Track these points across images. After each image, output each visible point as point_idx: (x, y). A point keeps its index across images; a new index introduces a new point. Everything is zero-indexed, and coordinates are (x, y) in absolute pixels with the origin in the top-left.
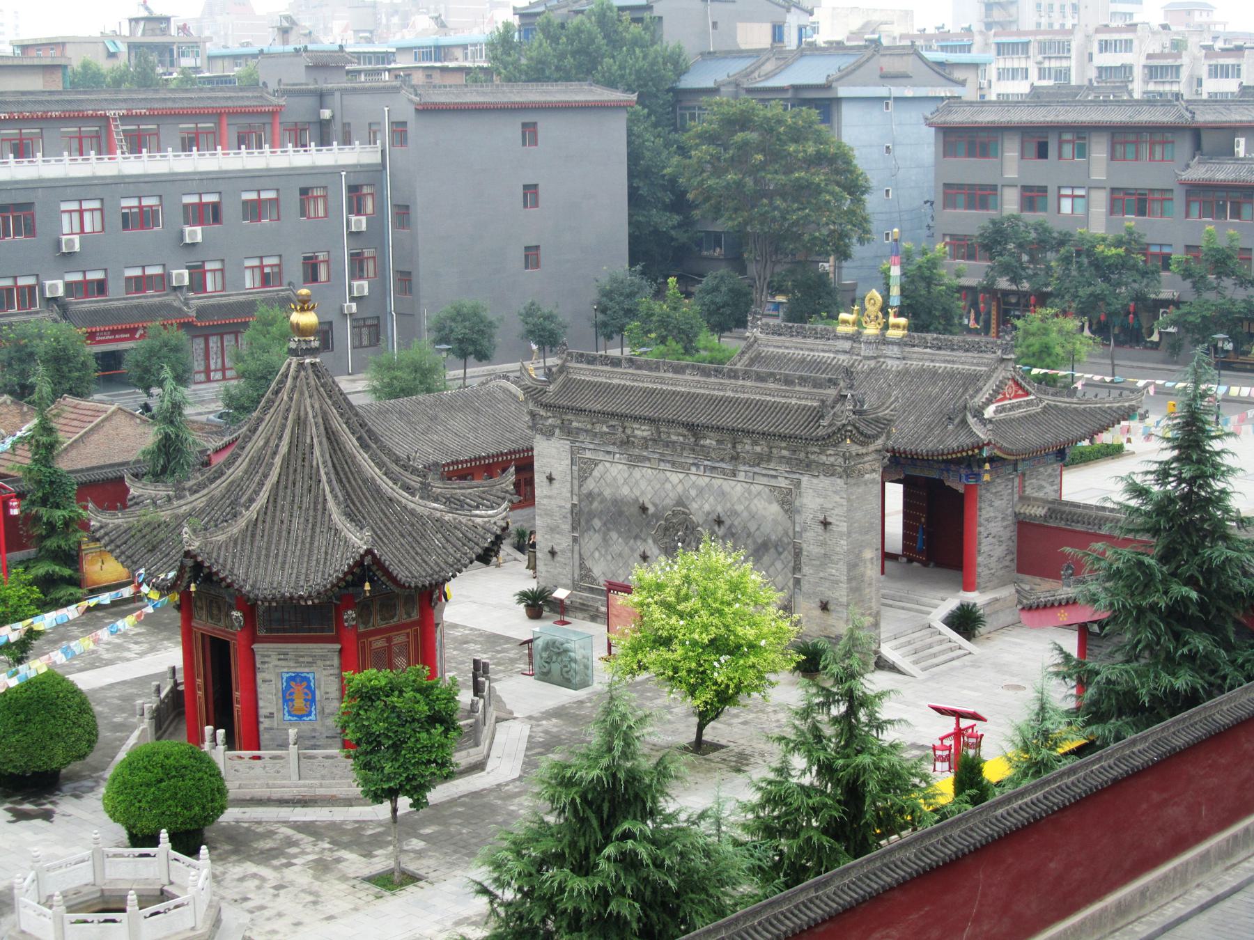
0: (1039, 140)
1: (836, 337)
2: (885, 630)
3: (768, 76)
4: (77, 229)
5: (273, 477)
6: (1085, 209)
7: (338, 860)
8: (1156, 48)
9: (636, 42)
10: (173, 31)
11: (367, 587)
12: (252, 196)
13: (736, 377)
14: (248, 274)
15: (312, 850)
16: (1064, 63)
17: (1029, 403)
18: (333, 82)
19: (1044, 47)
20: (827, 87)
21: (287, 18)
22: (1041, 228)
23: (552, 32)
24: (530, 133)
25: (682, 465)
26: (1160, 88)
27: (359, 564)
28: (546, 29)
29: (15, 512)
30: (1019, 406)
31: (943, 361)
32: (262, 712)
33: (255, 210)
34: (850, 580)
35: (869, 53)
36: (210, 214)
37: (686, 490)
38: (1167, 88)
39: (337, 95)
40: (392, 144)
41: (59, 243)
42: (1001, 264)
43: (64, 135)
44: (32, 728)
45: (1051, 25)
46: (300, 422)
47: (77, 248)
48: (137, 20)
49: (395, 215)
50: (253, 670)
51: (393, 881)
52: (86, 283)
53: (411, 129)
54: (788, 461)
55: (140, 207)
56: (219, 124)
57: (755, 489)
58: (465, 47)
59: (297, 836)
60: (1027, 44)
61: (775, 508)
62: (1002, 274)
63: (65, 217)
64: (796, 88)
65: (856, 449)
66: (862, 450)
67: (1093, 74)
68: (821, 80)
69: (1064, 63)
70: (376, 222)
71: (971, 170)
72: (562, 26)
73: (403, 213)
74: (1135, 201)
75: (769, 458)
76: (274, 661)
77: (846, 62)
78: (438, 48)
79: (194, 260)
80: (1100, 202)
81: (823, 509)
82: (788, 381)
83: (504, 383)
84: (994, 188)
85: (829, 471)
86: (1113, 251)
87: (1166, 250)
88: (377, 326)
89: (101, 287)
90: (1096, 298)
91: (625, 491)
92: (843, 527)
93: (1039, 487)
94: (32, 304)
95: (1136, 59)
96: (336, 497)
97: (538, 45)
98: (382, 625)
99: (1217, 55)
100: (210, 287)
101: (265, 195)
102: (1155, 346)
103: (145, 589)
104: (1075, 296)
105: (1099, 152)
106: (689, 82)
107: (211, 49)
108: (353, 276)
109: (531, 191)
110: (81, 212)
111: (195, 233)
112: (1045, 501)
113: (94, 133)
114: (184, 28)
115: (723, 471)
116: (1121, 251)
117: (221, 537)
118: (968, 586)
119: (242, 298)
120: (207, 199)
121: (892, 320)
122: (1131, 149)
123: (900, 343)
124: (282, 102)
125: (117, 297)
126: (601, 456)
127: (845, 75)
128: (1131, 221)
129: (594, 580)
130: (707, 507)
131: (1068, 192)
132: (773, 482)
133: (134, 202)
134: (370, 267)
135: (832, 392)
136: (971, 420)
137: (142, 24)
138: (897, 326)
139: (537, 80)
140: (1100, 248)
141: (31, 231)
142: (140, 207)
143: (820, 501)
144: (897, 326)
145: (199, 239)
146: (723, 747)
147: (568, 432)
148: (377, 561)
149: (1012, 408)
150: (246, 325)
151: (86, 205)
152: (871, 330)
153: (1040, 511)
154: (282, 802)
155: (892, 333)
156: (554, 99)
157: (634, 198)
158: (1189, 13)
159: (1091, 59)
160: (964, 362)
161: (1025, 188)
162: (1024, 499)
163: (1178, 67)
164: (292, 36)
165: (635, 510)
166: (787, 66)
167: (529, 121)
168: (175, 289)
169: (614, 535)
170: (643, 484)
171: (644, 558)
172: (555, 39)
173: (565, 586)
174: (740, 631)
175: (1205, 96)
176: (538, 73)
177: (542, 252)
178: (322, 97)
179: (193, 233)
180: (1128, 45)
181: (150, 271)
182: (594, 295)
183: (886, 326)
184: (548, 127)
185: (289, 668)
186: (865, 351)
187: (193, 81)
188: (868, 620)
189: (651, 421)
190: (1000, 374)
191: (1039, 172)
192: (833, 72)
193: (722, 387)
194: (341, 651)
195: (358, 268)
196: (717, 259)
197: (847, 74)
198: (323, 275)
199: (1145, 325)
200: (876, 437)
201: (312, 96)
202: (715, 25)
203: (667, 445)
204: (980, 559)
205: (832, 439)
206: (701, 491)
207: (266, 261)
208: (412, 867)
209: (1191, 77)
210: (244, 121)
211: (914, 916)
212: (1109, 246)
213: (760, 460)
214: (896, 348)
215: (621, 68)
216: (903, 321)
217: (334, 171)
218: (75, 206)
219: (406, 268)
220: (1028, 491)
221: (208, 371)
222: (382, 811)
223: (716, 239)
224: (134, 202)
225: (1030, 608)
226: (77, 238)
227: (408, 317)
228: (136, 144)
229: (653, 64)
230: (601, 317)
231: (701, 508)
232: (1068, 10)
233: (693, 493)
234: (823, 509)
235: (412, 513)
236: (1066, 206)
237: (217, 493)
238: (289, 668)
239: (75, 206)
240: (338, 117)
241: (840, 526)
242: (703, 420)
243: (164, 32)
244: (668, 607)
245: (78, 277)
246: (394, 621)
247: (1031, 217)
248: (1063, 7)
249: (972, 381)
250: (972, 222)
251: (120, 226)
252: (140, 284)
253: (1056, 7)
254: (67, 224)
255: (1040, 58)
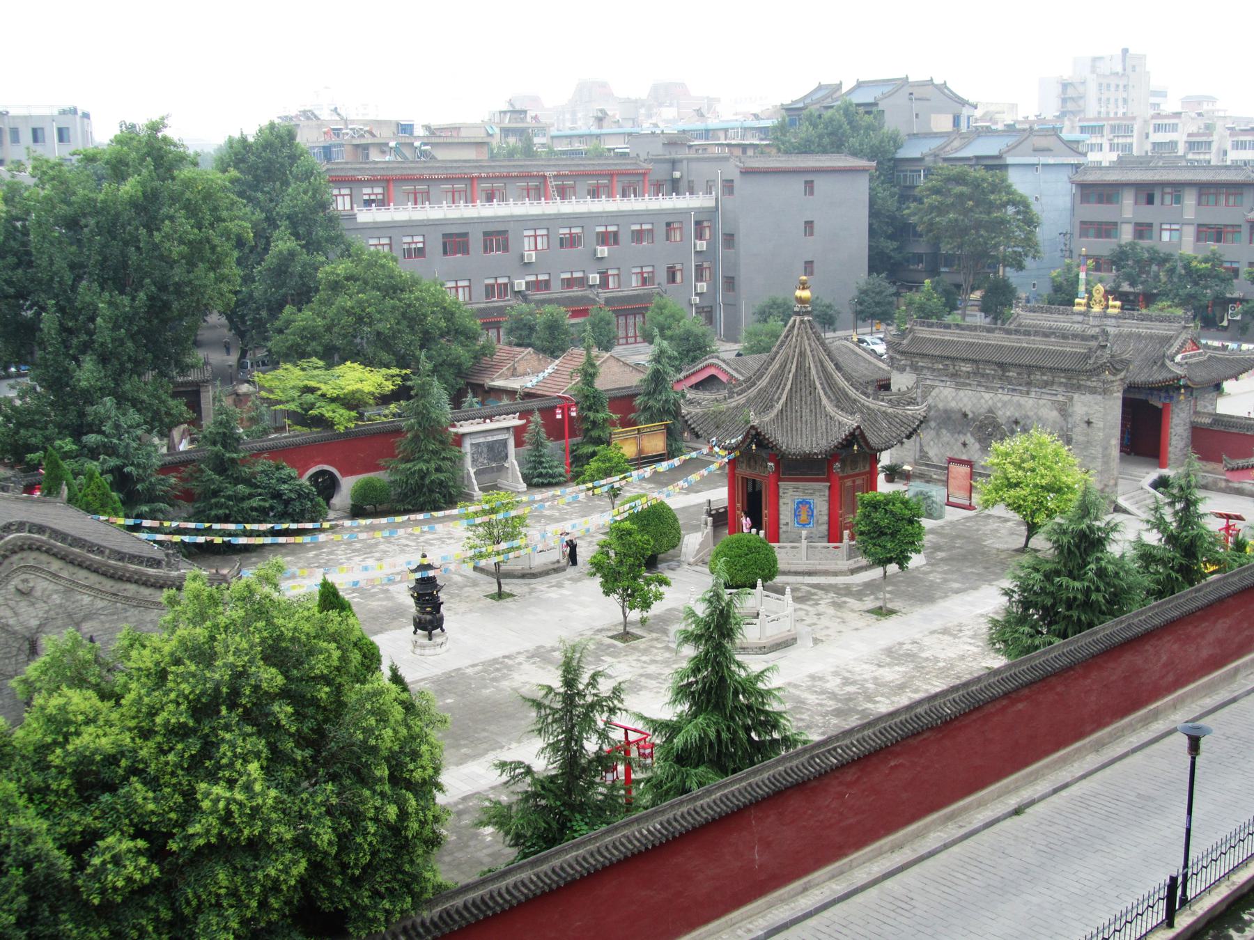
0: (1147, 193)
1: (1073, 313)
2: (1120, 489)
3: (957, 150)
4: (533, 247)
5: (788, 387)
6: (1179, 237)
7: (845, 602)
8: (1193, 129)
9: (869, 127)
10: (529, 119)
11: (856, 447)
12: (637, 227)
13: (1029, 335)
14: (634, 277)
15: (826, 600)
16: (1129, 140)
17: (1200, 354)
18: (682, 154)
19: (1114, 129)
20: (999, 157)
21: (601, 111)
22: (1151, 250)
23: (814, 120)
24: (809, 185)
25: (992, 388)
26: (1197, 157)
27: (852, 434)
28: (810, 118)
29: (574, 414)
30: (1194, 356)
31: (1143, 329)
32: (782, 522)
33: (639, 236)
34: (1104, 457)
35: (1026, 134)
36: (604, 239)
37: (995, 403)
38: (1202, 157)
39: (685, 162)
40: (723, 194)
41: (522, 256)
42: (1125, 273)
43: (404, 191)
44: (650, 528)
45: (1108, 113)
46: (802, 354)
47: (534, 259)
48: (505, 112)
49: (724, 240)
50: (777, 497)
51: (882, 612)
52: (538, 282)
53: (737, 184)
54: (1065, 385)
55: (571, 234)
56: (611, 181)
57: (1042, 402)
58: (726, 130)
59: (813, 591)
60: (1102, 127)
61: (1055, 414)
62: (1126, 280)
63: (526, 240)
64: (978, 158)
65: (1111, 378)
66: (1113, 378)
67: (1149, 147)
68: (996, 153)
69: (1129, 140)
70: (712, 244)
71: (1098, 212)
72: (820, 116)
73: (730, 239)
74: (1218, 233)
75: (1053, 383)
76: (790, 492)
77: (1011, 141)
78: (707, 131)
79: (602, 267)
80: (1189, 234)
81: (1087, 414)
82: (1064, 337)
83: (848, 344)
84: (1115, 224)
85: (1093, 391)
86: (1204, 265)
87: (1235, 265)
88: (711, 312)
89: (547, 284)
90: (1192, 297)
91: (953, 404)
92: (1101, 425)
93: (1203, 406)
94: (506, 295)
95: (1180, 137)
96: (829, 397)
97: (804, 131)
98: (851, 472)
99: (1237, 135)
100: (611, 286)
101: (645, 227)
102: (1225, 328)
103: (716, 449)
104: (1177, 295)
105: (1190, 200)
106: (902, 154)
107: (554, 132)
108: (697, 280)
109: (809, 225)
110: (536, 237)
111: (603, 251)
112: (1211, 414)
113: (537, 187)
114: (535, 118)
115: (1021, 392)
116: (1209, 265)
117: (767, 419)
118: (1162, 466)
119: (630, 293)
120: (610, 229)
121: (1111, 303)
122: (1212, 198)
123: (1115, 317)
124: (650, 166)
125: (556, 290)
126: (937, 383)
127: (1011, 149)
128: (1213, 246)
129: (929, 459)
130: (1008, 414)
131: (1167, 227)
132: (1054, 398)
133: (567, 231)
134: (707, 274)
135: (1094, 344)
136: (1168, 363)
137: (508, 115)
138: (1114, 307)
139: (805, 152)
140: (1194, 263)
141: (506, 249)
142: (571, 234)
143: (1085, 409)
144: (1114, 307)
145: (606, 255)
146: (868, 611)
147: (915, 368)
148: (862, 432)
149: (1191, 357)
150: (646, 309)
151: (538, 232)
152: (1097, 309)
153: (1207, 421)
154: (796, 573)
155: (1110, 311)
156: (822, 165)
157: (872, 232)
158: (1200, 103)
159: (1147, 137)
160: (1160, 329)
161: (1137, 224)
162: (1196, 413)
163: (1210, 143)
164: (605, 124)
165: (959, 416)
166: (969, 143)
167: (809, 178)
168: (591, 286)
169: (944, 431)
170: (965, 400)
171: (965, 445)
172: (815, 126)
173: (909, 464)
174: (1064, 479)
175: (1229, 163)
176: (805, 148)
177: (815, 265)
178: (674, 163)
179: (603, 251)
180: (1174, 128)
181: (576, 275)
182: (856, 293)
183: (1107, 307)
184: (820, 183)
185: (799, 496)
186: (1092, 321)
187: (556, 153)
188: (1112, 482)
189: (974, 361)
190: (1183, 336)
191: (1147, 214)
192: (1003, 147)
193: (1019, 341)
194: (830, 487)
195: (699, 277)
196: (920, 271)
197: (1014, 148)
198: (678, 278)
199: (1218, 315)
200: (1120, 371)
201: (668, 165)
202: (917, 115)
203: (983, 376)
204: (1170, 449)
205: (1096, 371)
206: (1004, 404)
207: (645, 270)
208: (889, 606)
209: (1219, 149)
210: (626, 179)
211: (1237, 614)
212: (1200, 262)
213: (1046, 384)
214: (1113, 320)
215: (861, 144)
216: (1118, 303)
217: (686, 212)
218: (532, 233)
219: (731, 275)
220: (1199, 409)
221: (627, 337)
222: (877, 572)
223: (919, 258)
224: (567, 231)
225: (1233, 470)
226: (533, 253)
227: (732, 307)
228: (563, 193)
229: (882, 142)
230: (859, 308)
231: (1004, 415)
232: (1120, 103)
233: (999, 405)
234: (1087, 414)
235: (868, 408)
236: (1166, 236)
237: (752, 395)
238: (799, 496)
239: (532, 233)
240: (685, 178)
241: (1098, 424)
242: (1009, 360)
243: (523, 120)
244: (1019, 467)
245: (533, 278)
246: (857, 471)
247: (1145, 243)
248: (1116, 100)
249: (1167, 340)
250: (1104, 247)
251: (482, 250)
252: (569, 283)
253: (1112, 101)
254: (527, 244)
255: (1111, 136)
